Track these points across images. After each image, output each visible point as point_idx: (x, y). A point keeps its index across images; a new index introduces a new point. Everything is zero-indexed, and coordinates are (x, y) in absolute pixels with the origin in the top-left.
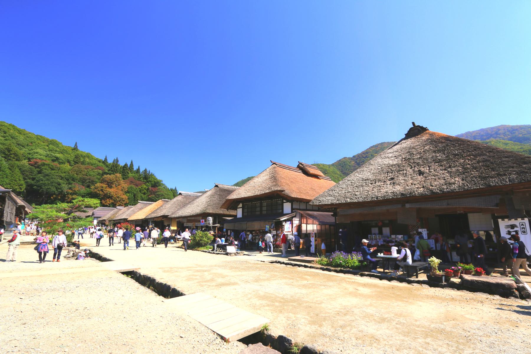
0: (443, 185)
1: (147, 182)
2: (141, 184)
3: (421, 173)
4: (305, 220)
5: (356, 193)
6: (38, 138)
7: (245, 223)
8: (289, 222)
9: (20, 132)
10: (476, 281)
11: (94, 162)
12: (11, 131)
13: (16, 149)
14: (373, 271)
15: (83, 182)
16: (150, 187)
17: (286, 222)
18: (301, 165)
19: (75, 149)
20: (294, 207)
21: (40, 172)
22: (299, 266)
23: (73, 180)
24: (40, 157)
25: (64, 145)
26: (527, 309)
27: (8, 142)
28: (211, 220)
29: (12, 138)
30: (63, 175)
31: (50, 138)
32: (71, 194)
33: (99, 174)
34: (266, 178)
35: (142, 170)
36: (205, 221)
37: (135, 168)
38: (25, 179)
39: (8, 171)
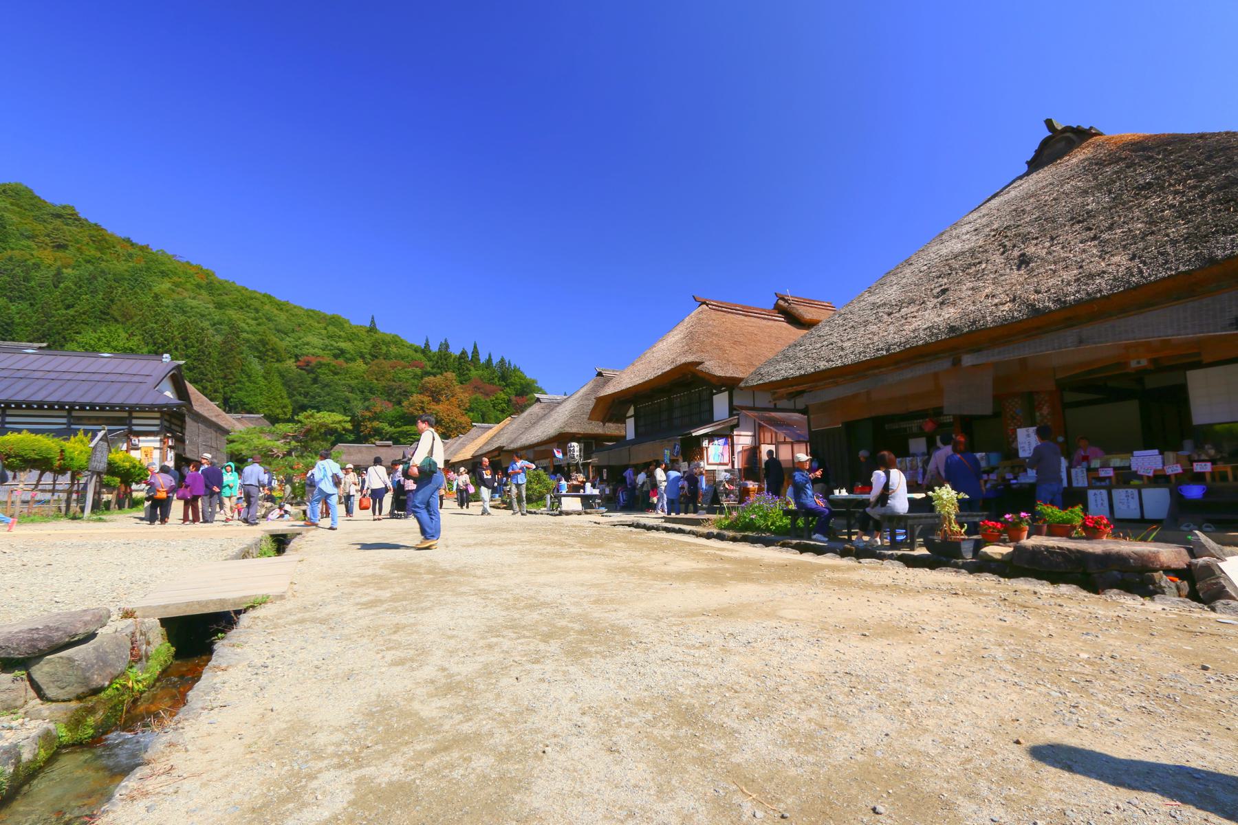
0: (1069, 284)
1: (507, 385)
2: (494, 392)
3: (1024, 261)
4: (768, 435)
5: (845, 345)
6: (311, 314)
7: (636, 452)
8: (722, 441)
9: (280, 307)
10: (1047, 548)
11: (406, 351)
12: (267, 307)
13: (274, 339)
14: (816, 536)
15: (389, 395)
16: (513, 398)
17: (711, 441)
18: (781, 302)
19: (372, 329)
20: (735, 403)
21: (315, 381)
22: (680, 531)
23: (371, 391)
24: (312, 351)
25: (353, 323)
26: (758, 564)
27: (261, 329)
28: (577, 449)
29: (269, 319)
30: (353, 383)
31: (329, 312)
32: (370, 419)
33: (415, 376)
34: (677, 338)
35: (495, 361)
36: (565, 454)
37: (483, 358)
38: (291, 396)
39: (262, 382)
